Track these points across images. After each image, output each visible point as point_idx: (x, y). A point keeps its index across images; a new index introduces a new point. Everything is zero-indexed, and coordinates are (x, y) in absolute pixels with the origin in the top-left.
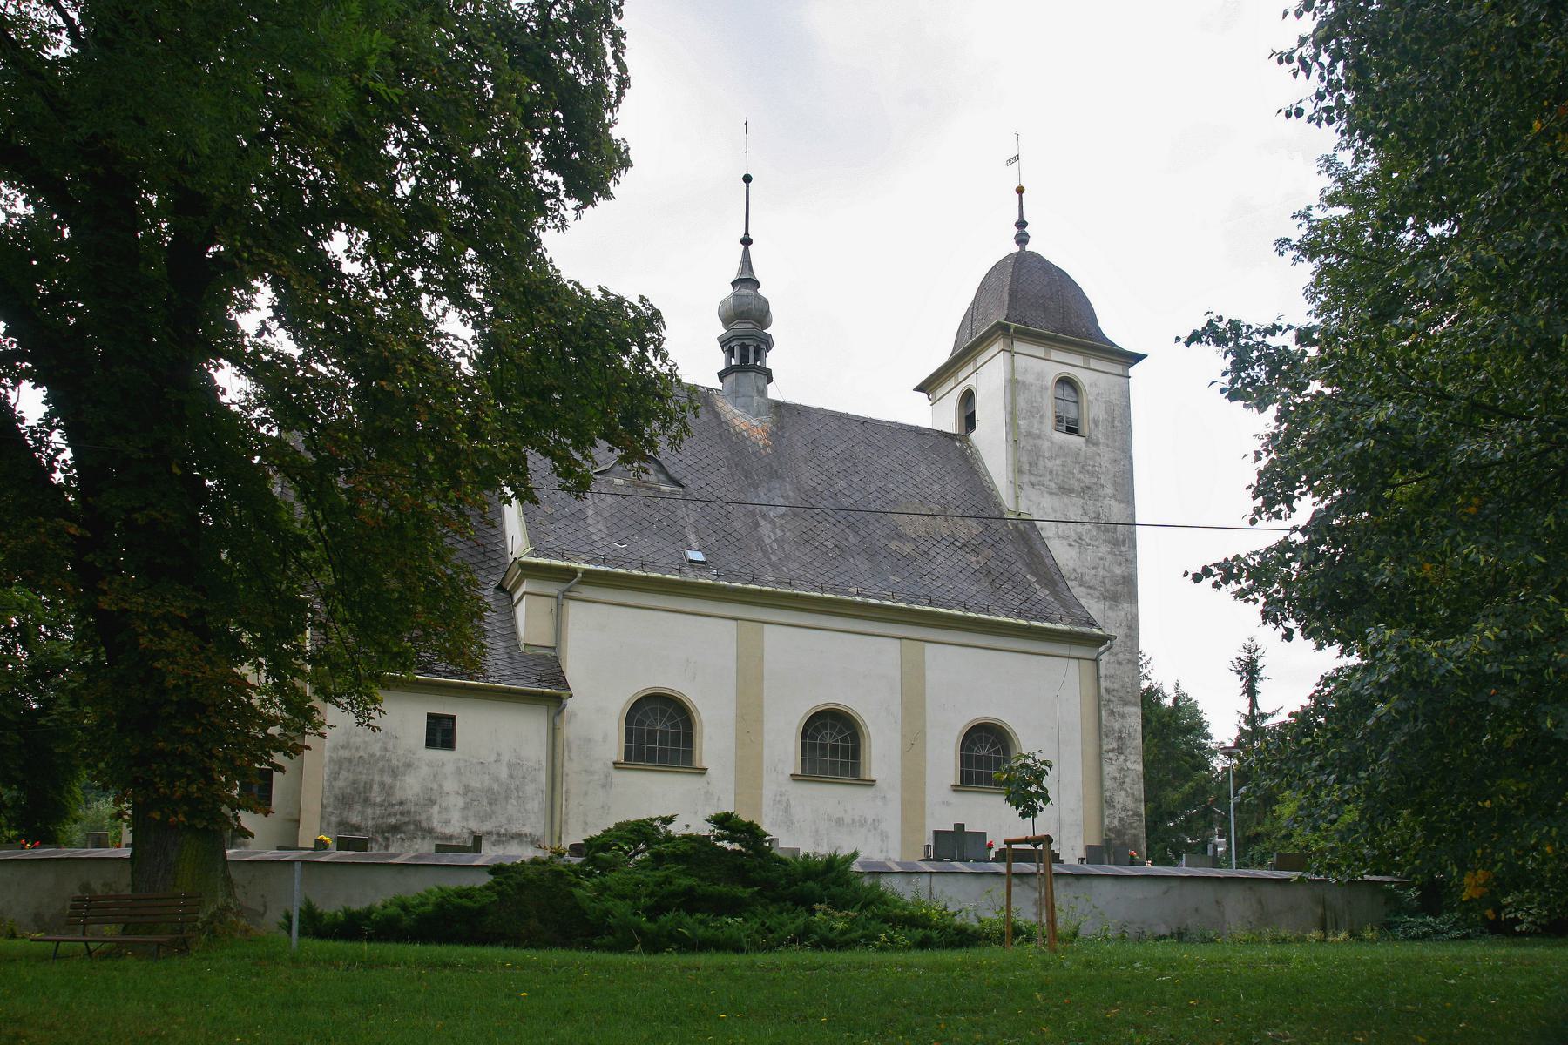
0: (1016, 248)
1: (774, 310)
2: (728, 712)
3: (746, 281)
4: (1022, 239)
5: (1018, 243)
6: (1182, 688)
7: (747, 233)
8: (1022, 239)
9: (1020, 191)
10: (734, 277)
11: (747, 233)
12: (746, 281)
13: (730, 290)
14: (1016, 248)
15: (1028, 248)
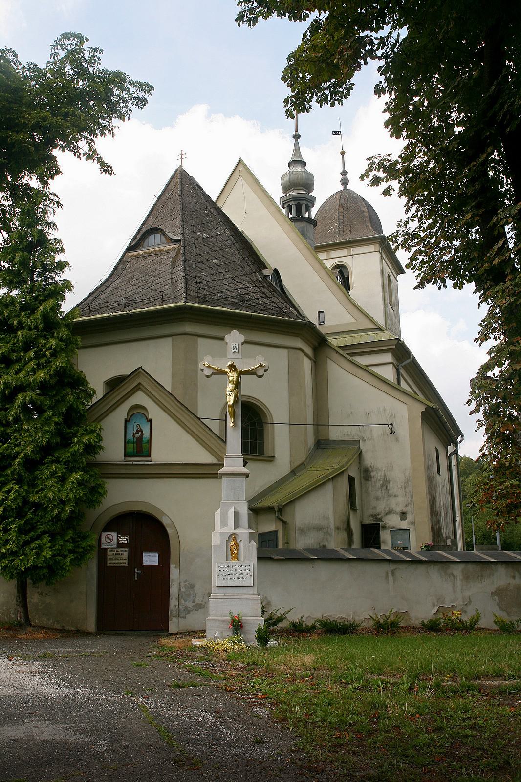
0: (342, 188)
1: (316, 185)
2: (409, 388)
3: (297, 162)
4: (345, 182)
5: (342, 184)
6: (468, 397)
7: (297, 132)
8: (345, 182)
9: (343, 153)
10: (289, 160)
11: (297, 132)
12: (297, 162)
13: (286, 169)
14: (342, 188)
15: (348, 187)
